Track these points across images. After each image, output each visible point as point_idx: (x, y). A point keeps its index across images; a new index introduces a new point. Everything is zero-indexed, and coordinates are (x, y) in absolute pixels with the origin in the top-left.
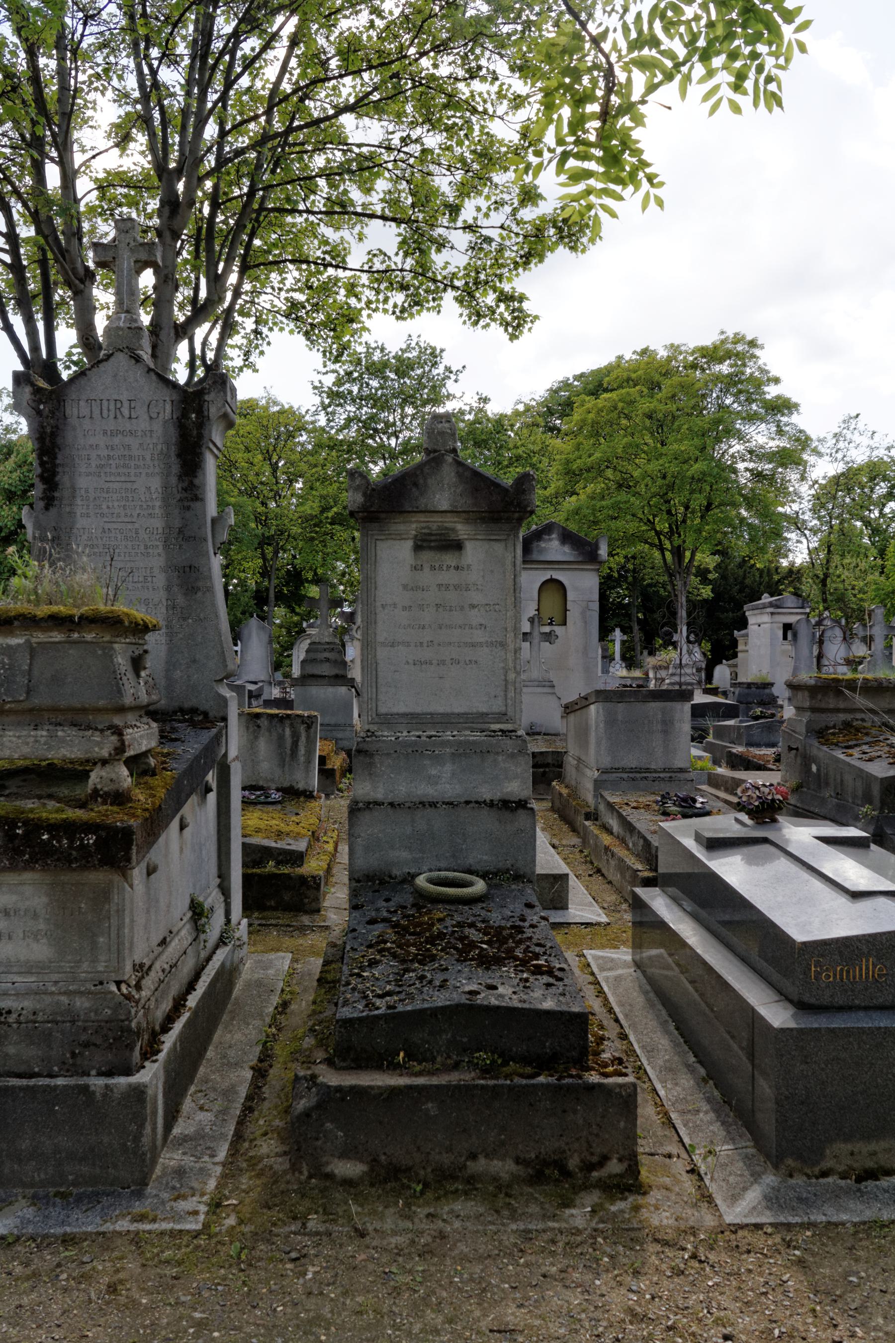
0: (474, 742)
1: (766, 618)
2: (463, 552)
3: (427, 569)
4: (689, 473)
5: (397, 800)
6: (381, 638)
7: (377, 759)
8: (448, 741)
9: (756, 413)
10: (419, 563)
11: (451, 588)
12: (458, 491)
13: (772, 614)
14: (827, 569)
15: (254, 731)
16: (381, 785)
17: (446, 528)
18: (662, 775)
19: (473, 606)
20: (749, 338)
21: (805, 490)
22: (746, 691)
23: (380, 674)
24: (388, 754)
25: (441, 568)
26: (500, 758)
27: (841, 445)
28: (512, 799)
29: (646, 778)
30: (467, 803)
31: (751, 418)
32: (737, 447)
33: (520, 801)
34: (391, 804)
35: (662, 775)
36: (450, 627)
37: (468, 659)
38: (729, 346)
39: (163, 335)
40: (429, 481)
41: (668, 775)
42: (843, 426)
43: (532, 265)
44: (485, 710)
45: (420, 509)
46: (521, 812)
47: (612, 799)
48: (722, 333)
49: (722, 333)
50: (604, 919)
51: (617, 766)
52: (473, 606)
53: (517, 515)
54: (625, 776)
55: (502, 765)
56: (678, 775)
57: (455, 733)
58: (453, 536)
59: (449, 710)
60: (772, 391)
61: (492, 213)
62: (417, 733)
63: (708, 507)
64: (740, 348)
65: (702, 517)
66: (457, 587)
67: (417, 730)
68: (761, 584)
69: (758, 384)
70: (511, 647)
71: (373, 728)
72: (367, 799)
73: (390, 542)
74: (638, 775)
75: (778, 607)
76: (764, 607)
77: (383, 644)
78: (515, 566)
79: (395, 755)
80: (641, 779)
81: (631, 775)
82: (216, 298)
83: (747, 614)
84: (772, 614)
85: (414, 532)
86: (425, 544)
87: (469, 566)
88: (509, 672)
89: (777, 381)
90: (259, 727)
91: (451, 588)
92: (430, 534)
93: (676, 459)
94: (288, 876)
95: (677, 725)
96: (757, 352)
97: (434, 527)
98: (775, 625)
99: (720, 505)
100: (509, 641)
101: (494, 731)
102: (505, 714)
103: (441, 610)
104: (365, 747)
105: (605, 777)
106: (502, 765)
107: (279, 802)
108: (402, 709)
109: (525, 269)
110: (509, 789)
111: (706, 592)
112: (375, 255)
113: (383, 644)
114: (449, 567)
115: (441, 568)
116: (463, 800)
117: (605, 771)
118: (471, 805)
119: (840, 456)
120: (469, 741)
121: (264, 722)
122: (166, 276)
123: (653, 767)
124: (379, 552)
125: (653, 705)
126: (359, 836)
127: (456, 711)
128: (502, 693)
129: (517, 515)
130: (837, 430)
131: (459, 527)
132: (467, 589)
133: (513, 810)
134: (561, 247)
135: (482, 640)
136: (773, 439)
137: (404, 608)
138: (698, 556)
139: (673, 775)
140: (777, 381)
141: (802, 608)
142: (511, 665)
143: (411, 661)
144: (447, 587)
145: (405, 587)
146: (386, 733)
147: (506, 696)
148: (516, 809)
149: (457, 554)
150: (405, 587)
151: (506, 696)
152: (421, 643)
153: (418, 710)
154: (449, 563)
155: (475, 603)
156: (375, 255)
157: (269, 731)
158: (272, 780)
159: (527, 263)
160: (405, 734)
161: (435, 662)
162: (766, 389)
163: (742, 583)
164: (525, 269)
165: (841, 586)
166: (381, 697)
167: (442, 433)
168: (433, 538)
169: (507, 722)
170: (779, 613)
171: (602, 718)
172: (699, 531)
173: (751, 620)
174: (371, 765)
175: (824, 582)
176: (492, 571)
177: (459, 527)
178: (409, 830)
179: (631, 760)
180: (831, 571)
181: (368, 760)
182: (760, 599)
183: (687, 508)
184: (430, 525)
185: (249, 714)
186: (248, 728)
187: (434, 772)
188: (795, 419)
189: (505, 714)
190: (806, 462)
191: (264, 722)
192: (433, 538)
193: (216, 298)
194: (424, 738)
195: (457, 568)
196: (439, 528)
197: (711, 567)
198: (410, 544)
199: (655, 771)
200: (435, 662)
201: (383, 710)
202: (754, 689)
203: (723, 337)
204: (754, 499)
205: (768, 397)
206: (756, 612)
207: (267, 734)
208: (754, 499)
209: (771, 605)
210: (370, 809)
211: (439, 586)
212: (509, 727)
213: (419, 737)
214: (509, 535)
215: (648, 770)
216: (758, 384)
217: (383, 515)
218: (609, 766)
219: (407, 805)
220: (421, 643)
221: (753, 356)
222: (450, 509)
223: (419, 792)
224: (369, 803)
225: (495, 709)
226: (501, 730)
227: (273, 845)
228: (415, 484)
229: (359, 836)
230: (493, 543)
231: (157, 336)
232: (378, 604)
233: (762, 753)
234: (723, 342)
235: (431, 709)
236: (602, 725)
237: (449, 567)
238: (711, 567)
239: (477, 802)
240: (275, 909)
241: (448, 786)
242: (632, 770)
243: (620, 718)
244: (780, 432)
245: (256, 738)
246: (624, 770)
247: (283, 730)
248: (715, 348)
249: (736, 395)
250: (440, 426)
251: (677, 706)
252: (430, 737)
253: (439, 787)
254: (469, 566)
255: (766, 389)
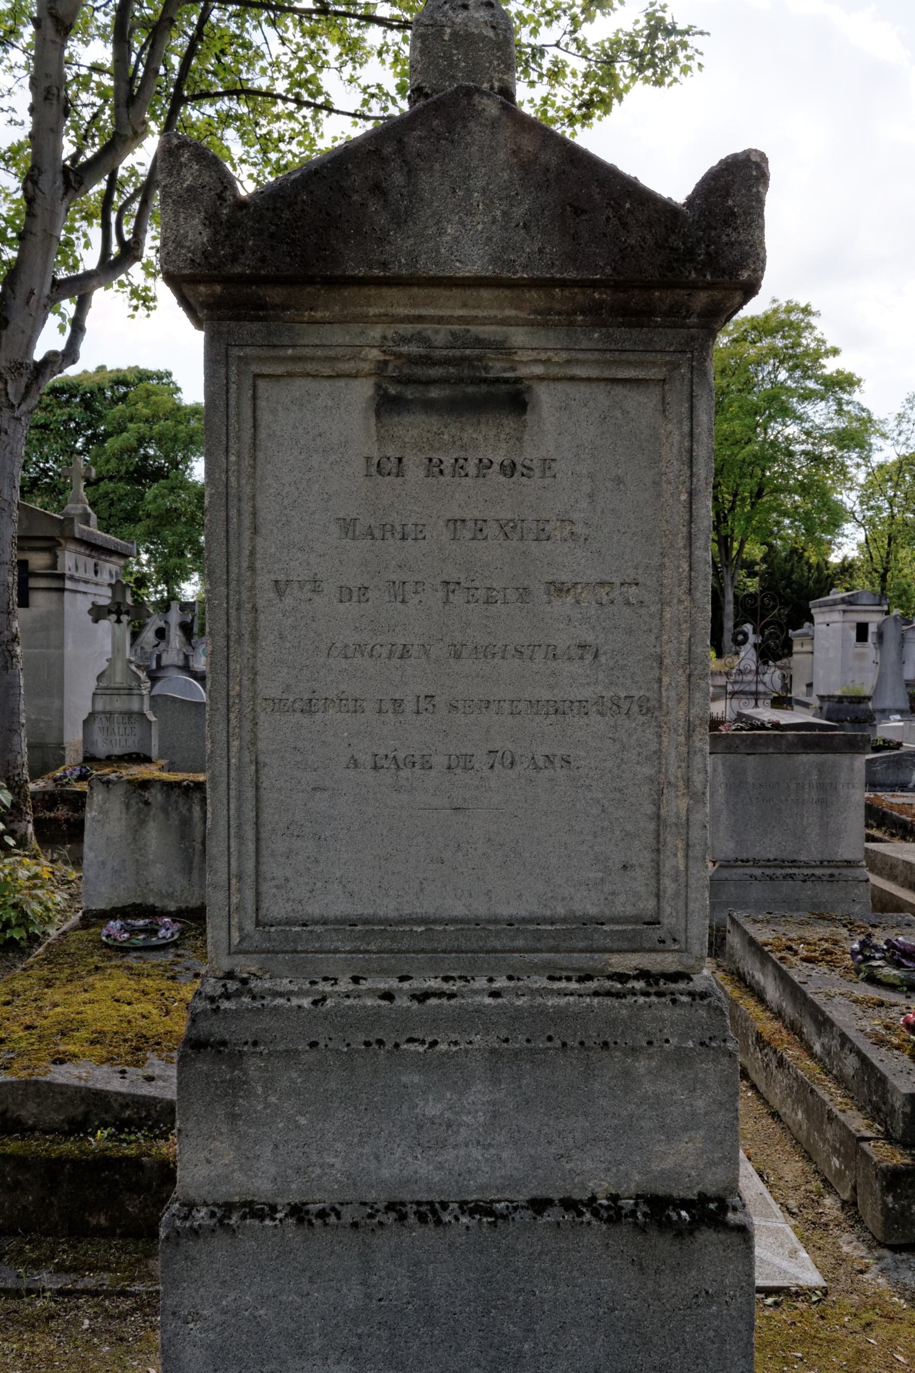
0: (560, 1014)
1: (836, 616)
2: (528, 417)
3: (415, 469)
4: (740, 457)
5: (318, 1200)
6: (269, 688)
7: (253, 1066)
8: (479, 1010)
9: (812, 391)
10: (392, 452)
11: (492, 530)
12: (519, 212)
13: (844, 611)
14: (888, 563)
15: (139, 812)
16: (267, 1151)
17: (479, 342)
18: (818, 872)
19: (559, 589)
20: (803, 305)
21: (861, 477)
22: (837, 706)
23: (267, 796)
24: (290, 1054)
25: (459, 467)
26: (642, 1066)
27: (904, 426)
28: (679, 1192)
29: (792, 876)
30: (539, 1205)
31: (807, 396)
32: (792, 430)
33: (704, 1198)
34: (298, 1212)
35: (818, 872)
36: (485, 652)
37: (542, 750)
38: (783, 316)
39: (45, 182)
40: (425, 181)
41: (828, 871)
42: (908, 406)
43: (594, 120)
44: (593, 910)
45: (394, 270)
46: (707, 1236)
47: (763, 934)
48: (774, 301)
49: (774, 301)
50: (812, 1277)
51: (744, 856)
52: (559, 589)
53: (702, 299)
54: (757, 872)
55: (648, 1087)
56: (844, 871)
57: (501, 983)
58: (497, 368)
59: (481, 909)
60: (830, 366)
61: (543, 29)
62: (383, 985)
63: (759, 494)
64: (793, 317)
65: (753, 505)
66: (507, 529)
67: (384, 972)
68: (809, 579)
69: (817, 356)
70: (678, 714)
71: (246, 965)
72: (224, 1193)
73: (300, 386)
74: (779, 872)
75: (851, 604)
76: (835, 603)
77: (278, 705)
78: (691, 463)
79: (310, 1057)
80: (785, 877)
81: (768, 871)
82: (130, 133)
83: (813, 611)
84: (844, 611)
85: (375, 354)
86: (410, 393)
87: (547, 463)
88: (669, 793)
89: (835, 352)
90: (147, 803)
91: (492, 530)
92: (427, 361)
93: (726, 440)
94: (134, 1163)
95: (843, 792)
96: (813, 320)
97: (440, 335)
98: (847, 625)
99: (772, 492)
100: (670, 696)
101: (622, 978)
102: (655, 922)
103: (458, 598)
104: (216, 1029)
105: (725, 873)
106: (648, 1087)
107: (175, 944)
108: (341, 907)
109: (583, 125)
110: (668, 1164)
111: (753, 585)
112: (373, 96)
113: (278, 705)
114: (484, 466)
115: (459, 467)
116: (522, 1197)
117: (727, 865)
118: (550, 1216)
119: (902, 439)
120: (542, 1011)
121: (155, 796)
122: (48, 90)
123: (803, 858)
124: (265, 417)
125: (804, 758)
126: (196, 1316)
127: (505, 911)
128: (646, 857)
129: (702, 299)
130: (901, 411)
131: (518, 337)
132: (542, 536)
133: (682, 1232)
134: (639, 83)
135: (587, 693)
136: (831, 420)
137: (345, 594)
138: (747, 547)
139: (836, 871)
140: (835, 352)
141: (880, 605)
142: (674, 771)
143: (366, 759)
144: (480, 526)
145: (348, 526)
146: (284, 984)
147: (657, 866)
148: (692, 1228)
149: (509, 424)
150: (348, 526)
151: (657, 866)
152: (397, 703)
153: (388, 908)
154: (487, 453)
155: (565, 577)
156: (373, 96)
157: (165, 811)
158: (171, 896)
159: (587, 117)
160: (345, 985)
161: (439, 761)
162: (823, 361)
163: (789, 578)
164: (583, 125)
165: (904, 581)
166: (270, 867)
167: (464, 39)
168: (435, 372)
169: (660, 946)
170: (852, 611)
171: (721, 779)
172: (749, 519)
173: (818, 618)
174: (237, 1087)
175: (883, 578)
176: (619, 480)
177: (518, 337)
178: (353, 1296)
179: (766, 849)
180: (892, 564)
181: (225, 1071)
182: (828, 594)
183: (735, 495)
184: (428, 329)
185: (129, 782)
186: (128, 806)
187: (433, 1109)
188: (856, 397)
189: (655, 922)
190: (871, 445)
191: (155, 796)
192: (435, 372)
193: (130, 133)
194: (403, 1002)
195: (510, 469)
196: (456, 340)
197: (758, 559)
198: (364, 389)
199: (807, 865)
200: (439, 761)
201: (276, 909)
202: (846, 704)
203: (775, 306)
204: (811, 485)
205: (827, 372)
206: (824, 609)
207: (161, 816)
208: (811, 485)
209: (843, 601)
210: (232, 1231)
211: (455, 522)
212: (667, 962)
213: (388, 996)
214: (675, 366)
215: (794, 863)
216: (817, 356)
217: (274, 295)
218: (732, 856)
219: (348, 1215)
220: (397, 703)
221: (809, 326)
222: (489, 271)
223: (385, 1173)
224: (229, 1208)
225: (623, 906)
226: (643, 974)
227: (116, 1085)
228: (378, 189)
229: (196, 1316)
230: (619, 390)
231: (35, 183)
232: (264, 580)
233: (900, 801)
234: (775, 311)
235: (427, 907)
236: (721, 791)
237: (484, 466)
238: (758, 559)
239: (569, 1204)
240: (106, 1233)
241: (476, 1153)
242: (769, 863)
243: (750, 779)
244: (840, 412)
245: (142, 823)
246: (756, 863)
247: (190, 810)
248: (767, 318)
249: (791, 370)
250: (460, 17)
251: (843, 760)
252: (422, 997)
253: (449, 1155)
254: (547, 463)
255: (823, 361)
